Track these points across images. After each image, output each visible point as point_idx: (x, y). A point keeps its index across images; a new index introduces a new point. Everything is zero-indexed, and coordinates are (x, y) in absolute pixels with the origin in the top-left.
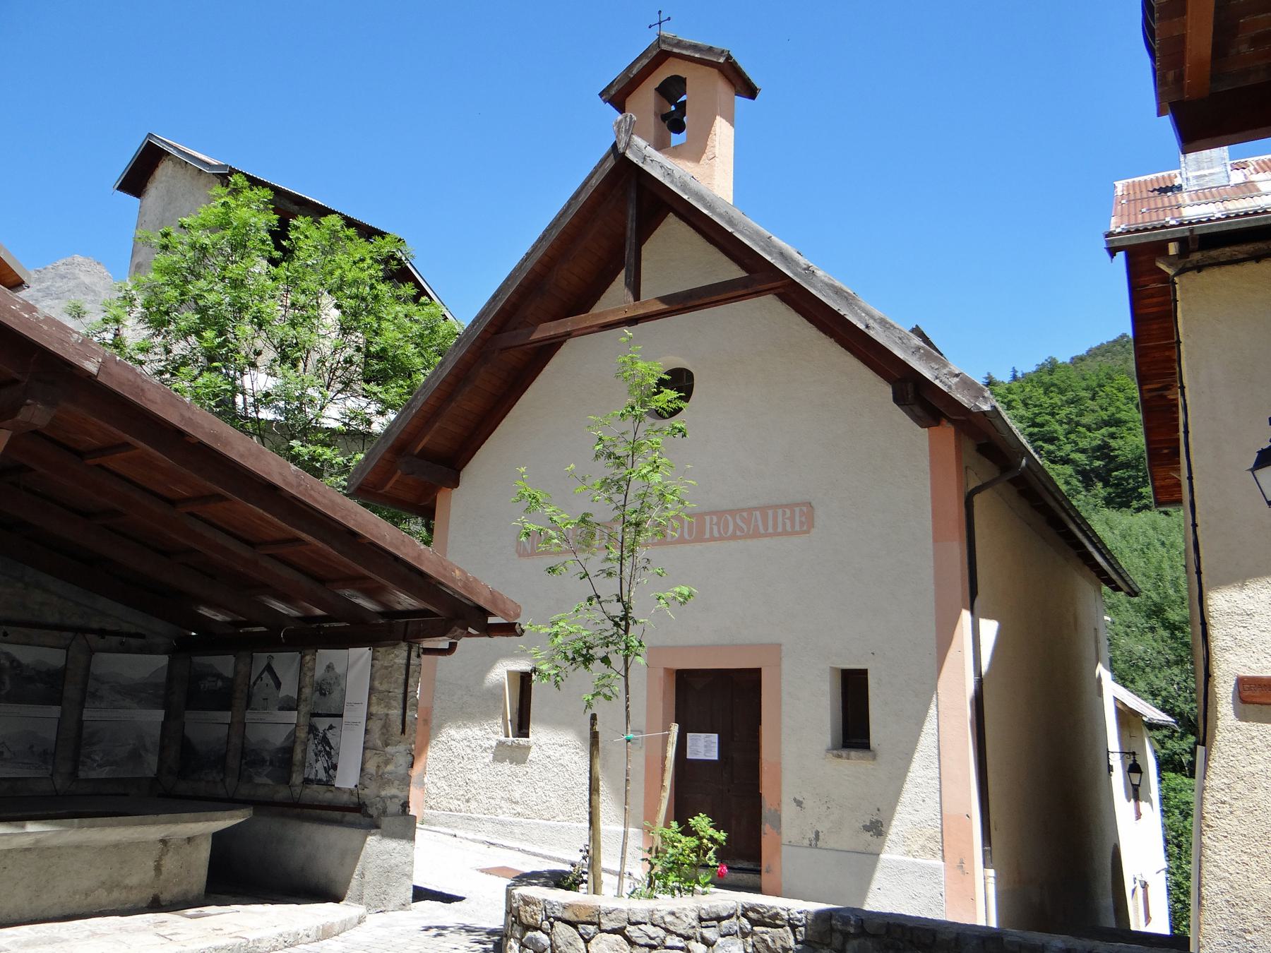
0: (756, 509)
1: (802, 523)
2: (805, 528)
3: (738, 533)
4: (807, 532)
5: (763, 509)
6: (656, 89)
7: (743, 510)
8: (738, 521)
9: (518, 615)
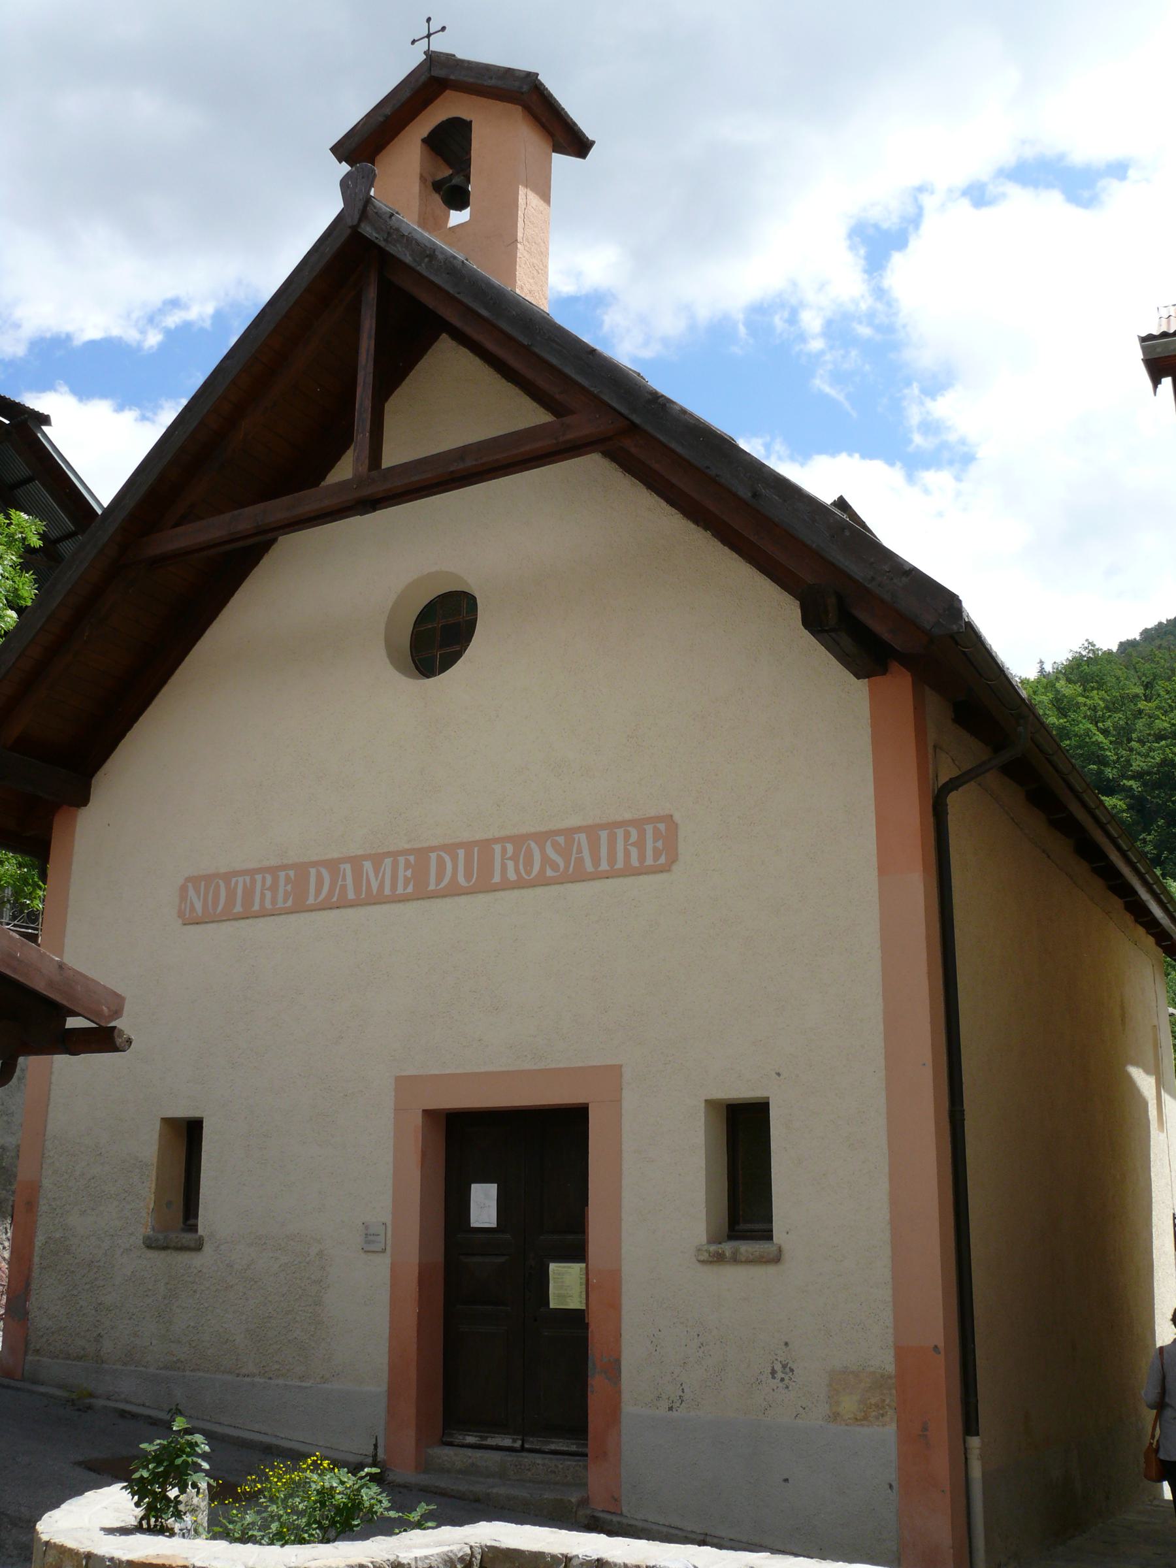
0: (579, 829)
1: (657, 854)
2: (662, 860)
3: (550, 873)
4: (665, 869)
5: (592, 831)
6: (424, 141)
7: (558, 832)
8: (550, 851)
9: (117, 1013)
